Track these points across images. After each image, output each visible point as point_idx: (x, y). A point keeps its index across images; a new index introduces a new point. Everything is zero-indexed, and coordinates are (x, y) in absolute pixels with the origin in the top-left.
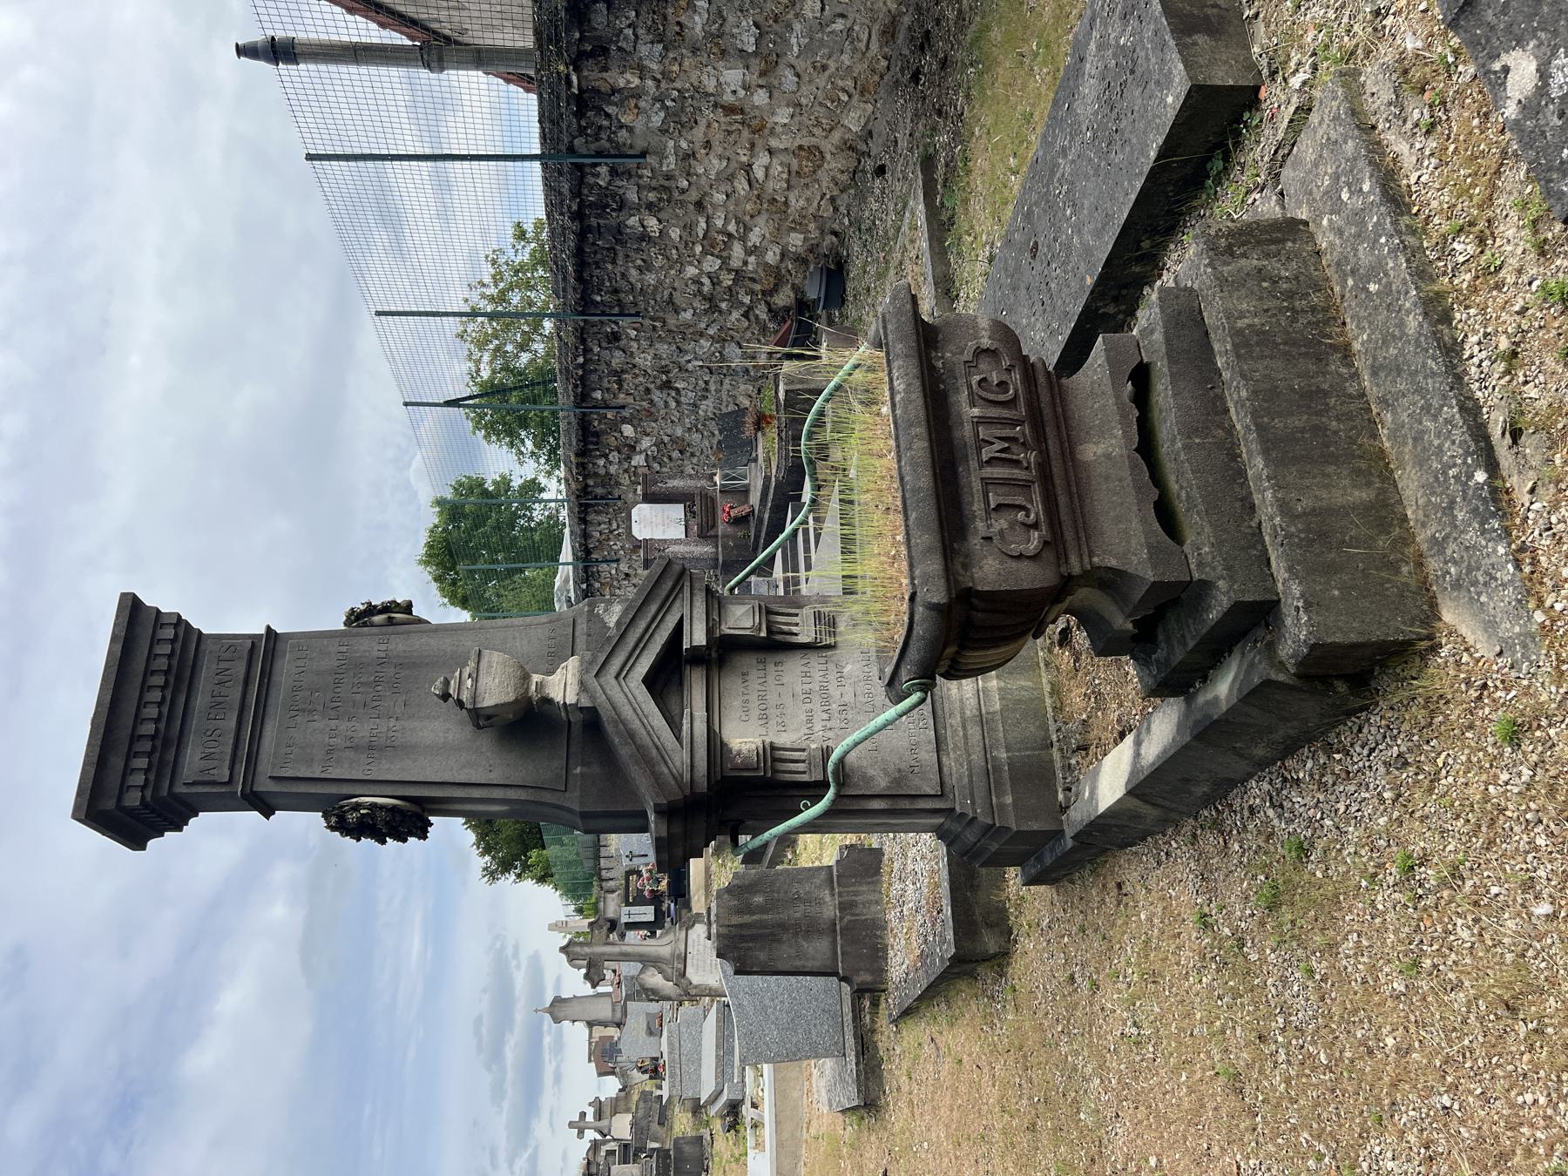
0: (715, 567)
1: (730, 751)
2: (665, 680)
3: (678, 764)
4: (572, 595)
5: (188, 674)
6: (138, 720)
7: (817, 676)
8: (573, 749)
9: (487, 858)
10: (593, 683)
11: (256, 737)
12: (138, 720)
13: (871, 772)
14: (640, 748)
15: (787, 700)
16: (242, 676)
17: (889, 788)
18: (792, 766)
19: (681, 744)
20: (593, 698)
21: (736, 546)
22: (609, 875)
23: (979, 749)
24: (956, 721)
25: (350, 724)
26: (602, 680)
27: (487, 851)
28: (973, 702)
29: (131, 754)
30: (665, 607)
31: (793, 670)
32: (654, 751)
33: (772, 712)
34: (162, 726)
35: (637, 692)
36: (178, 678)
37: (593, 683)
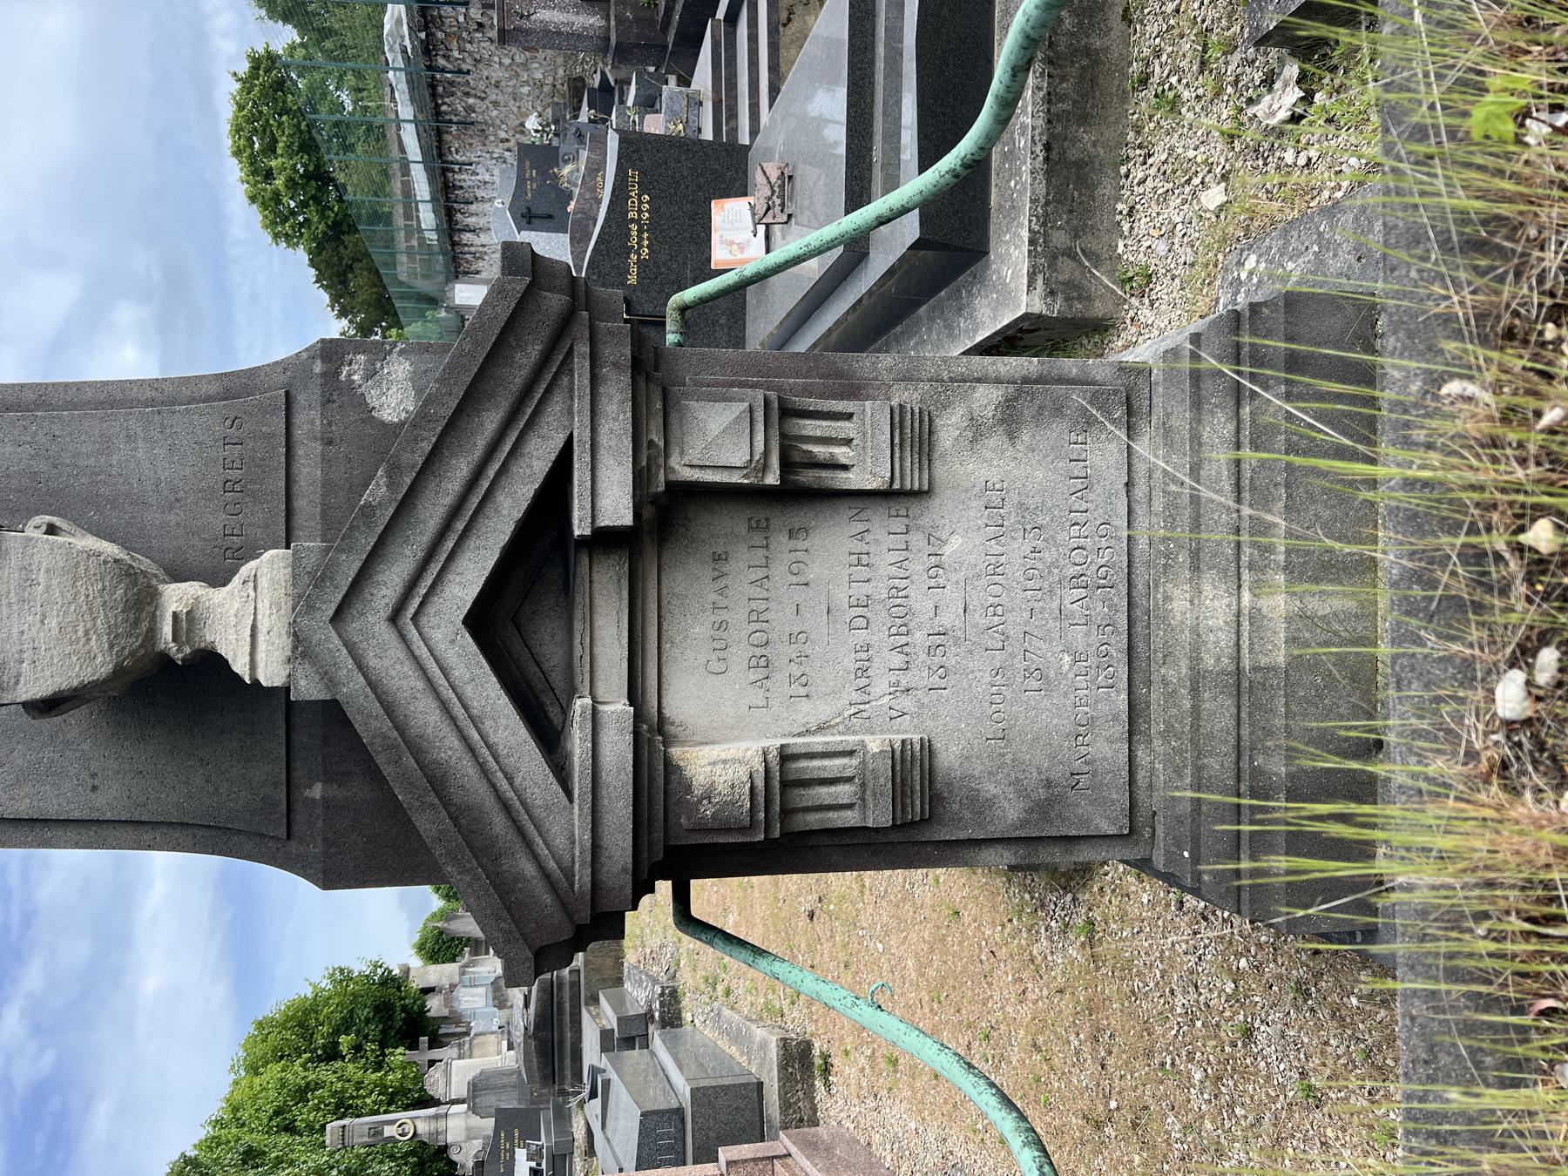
0: (604, 50)
1: (688, 788)
2: (518, 616)
3: (560, 842)
4: (407, 43)
7: (884, 561)
8: (301, 737)
9: (345, 322)
13: (990, 789)
14: (461, 816)
15: (816, 623)
17: (1024, 823)
18: (824, 794)
19: (569, 794)
20: (331, 682)
21: (637, 19)
23: (1227, 748)
24: (1177, 672)
26: (353, 627)
27: (343, 314)
28: (1225, 639)
30: (524, 413)
31: (831, 553)
32: (499, 822)
33: (782, 652)
35: (451, 655)
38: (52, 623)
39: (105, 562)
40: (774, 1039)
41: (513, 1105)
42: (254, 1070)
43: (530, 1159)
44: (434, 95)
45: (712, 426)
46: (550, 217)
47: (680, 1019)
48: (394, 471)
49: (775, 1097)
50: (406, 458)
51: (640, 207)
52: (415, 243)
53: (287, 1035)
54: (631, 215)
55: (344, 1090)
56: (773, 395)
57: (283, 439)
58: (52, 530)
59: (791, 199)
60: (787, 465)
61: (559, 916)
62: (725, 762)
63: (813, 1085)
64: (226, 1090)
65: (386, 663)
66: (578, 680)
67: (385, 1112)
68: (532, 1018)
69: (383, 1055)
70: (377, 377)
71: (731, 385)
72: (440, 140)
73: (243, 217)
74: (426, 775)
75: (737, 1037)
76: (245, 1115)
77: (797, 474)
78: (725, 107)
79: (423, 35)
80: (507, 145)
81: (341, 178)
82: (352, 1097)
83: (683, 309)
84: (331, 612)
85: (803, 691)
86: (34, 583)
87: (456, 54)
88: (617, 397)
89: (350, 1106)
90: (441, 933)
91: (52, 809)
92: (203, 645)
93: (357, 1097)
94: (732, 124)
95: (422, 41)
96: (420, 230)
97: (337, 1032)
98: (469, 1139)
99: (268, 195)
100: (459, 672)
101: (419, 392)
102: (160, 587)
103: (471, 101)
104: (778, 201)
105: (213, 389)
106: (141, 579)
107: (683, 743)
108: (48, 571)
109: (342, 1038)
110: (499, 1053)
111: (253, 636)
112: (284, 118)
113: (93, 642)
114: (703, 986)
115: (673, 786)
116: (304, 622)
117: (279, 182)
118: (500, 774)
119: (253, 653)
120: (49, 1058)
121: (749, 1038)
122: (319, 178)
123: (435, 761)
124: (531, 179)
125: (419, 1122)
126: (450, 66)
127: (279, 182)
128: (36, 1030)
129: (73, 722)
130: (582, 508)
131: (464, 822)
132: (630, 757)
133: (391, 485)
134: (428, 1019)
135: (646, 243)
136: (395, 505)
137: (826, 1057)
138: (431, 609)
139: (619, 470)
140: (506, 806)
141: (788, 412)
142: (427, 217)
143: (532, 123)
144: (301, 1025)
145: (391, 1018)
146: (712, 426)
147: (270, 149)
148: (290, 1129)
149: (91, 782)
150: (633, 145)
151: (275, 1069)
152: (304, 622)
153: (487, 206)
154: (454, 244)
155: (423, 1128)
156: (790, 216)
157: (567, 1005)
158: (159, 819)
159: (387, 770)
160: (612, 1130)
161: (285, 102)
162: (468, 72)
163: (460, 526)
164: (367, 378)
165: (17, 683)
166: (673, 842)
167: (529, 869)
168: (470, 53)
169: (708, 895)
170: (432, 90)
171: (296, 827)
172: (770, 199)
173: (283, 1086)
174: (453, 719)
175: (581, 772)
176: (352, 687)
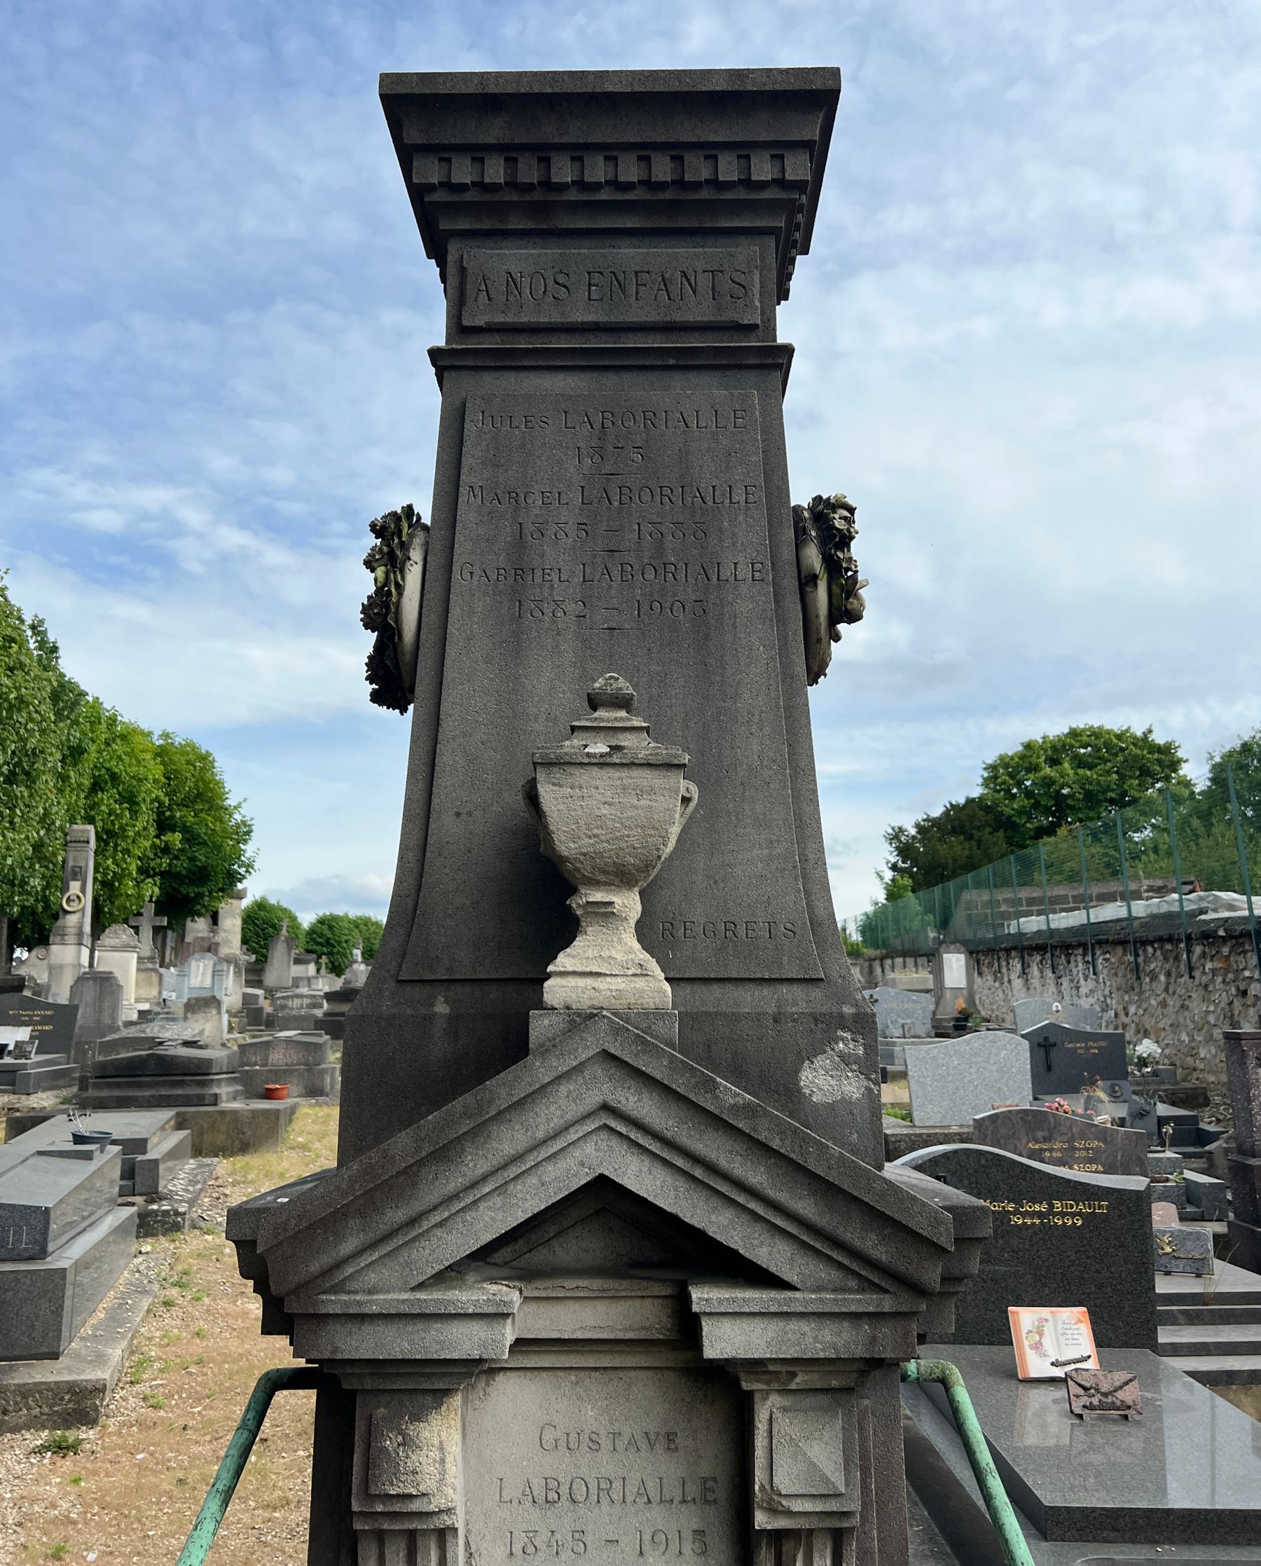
0: (1241, 1151)
1: (417, 1418)
3: (372, 1278)
4: (1211, 916)
5: (683, 223)
6: (578, 151)
9: (913, 831)
10: (587, 1046)
11: (549, 362)
12: (578, 151)
14: (410, 1175)
16: (679, 317)
19: (420, 1286)
20: (549, 1048)
22: (887, 967)
25: (571, 528)
26: (598, 1070)
29: (509, 152)
30: (815, 1240)
32: (398, 1215)
34: (573, 195)
35: (568, 1161)
36: (674, 207)
37: (587, 1046)
38: (605, 810)
39: (658, 850)
40: (107, 1377)
41: (80, 1020)
42: (162, 753)
43: (18, 1044)
44: (1161, 940)
45: (816, 1448)
46: (1049, 1068)
47: (146, 1236)
48: (750, 1111)
49: (38, 1378)
50: (763, 1123)
51: (1068, 1215)
52: (1004, 908)
53: (190, 784)
54: (1057, 1204)
55: (125, 838)
56: (856, 1521)
57: (777, 976)
58: (686, 800)
59: (1100, 1418)
60: (777, 1537)
61: (294, 1280)
62: (443, 1461)
63: (44, 1427)
64: (144, 725)
65: (562, 1102)
66: (540, 1284)
67: (95, 879)
68: (172, 1052)
69: (155, 874)
70: (842, 1066)
71: (865, 1470)
72: (1116, 943)
73: (1010, 734)
74: (450, 1142)
75: (115, 1318)
76: (118, 747)
77: (769, 1546)
78: (1203, 1309)
79: (1221, 933)
80: (1122, 1013)
81: (1062, 831)
82: (116, 845)
83: (944, 1382)
84: (612, 1051)
85: (517, 1548)
86: (639, 797)
87: (1209, 966)
88: (839, 1342)
89: (107, 843)
90: (274, 926)
91: (441, 782)
92: (584, 924)
93: (115, 850)
94: (1181, 1318)
95: (1215, 932)
96: (1018, 915)
97: (186, 830)
98: (51, 969)
99: (1034, 760)
100: (551, 1171)
101: (831, 1107)
102: (636, 890)
103: (1162, 978)
104: (1095, 1401)
105: (820, 911)
106: (643, 875)
107: (465, 1402)
108: (650, 807)
109: (178, 836)
110: (137, 1001)
111: (591, 974)
112: (1115, 776)
113: (588, 840)
114: (179, 1268)
115: (420, 1398)
116: (603, 1025)
117: (1047, 770)
118: (446, 1214)
119: (574, 973)
120: (196, 568)
121: (111, 1340)
122: (1060, 808)
123: (463, 1151)
124: (1087, 1048)
125: (79, 915)
126: (1194, 958)
127: (1047, 770)
128: (225, 558)
129: (516, 800)
130: (720, 1301)
131: (401, 1180)
132: (455, 1356)
133: (735, 1108)
134: (185, 920)
135: (1029, 1222)
136: (717, 1112)
137: (74, 1448)
138: (614, 1142)
139: (762, 1343)
140: (413, 1222)
141: (838, 1538)
142: (1032, 924)
143: (1146, 1047)
144: (199, 795)
145: (192, 882)
146: (816, 1448)
147: (1080, 763)
148: (96, 786)
149: (463, 811)
150: (1137, 1204)
151: (157, 771)
152: (603, 1025)
153: (1052, 988)
154: (1008, 951)
155: (72, 920)
156: (1080, 1417)
157: (180, 1092)
158: (426, 866)
159: (457, 1105)
160: (33, 1168)
161: (1131, 777)
162: (1192, 977)
163: (698, 1172)
164: (842, 1056)
165: (554, 784)
166: (359, 1400)
167: (347, 1248)
168: (1212, 980)
169: (297, 1408)
170: (1169, 937)
171: (408, 988)
172: (1097, 1390)
173: (140, 780)
174: (504, 1166)
175: (442, 1302)
176: (538, 1070)
